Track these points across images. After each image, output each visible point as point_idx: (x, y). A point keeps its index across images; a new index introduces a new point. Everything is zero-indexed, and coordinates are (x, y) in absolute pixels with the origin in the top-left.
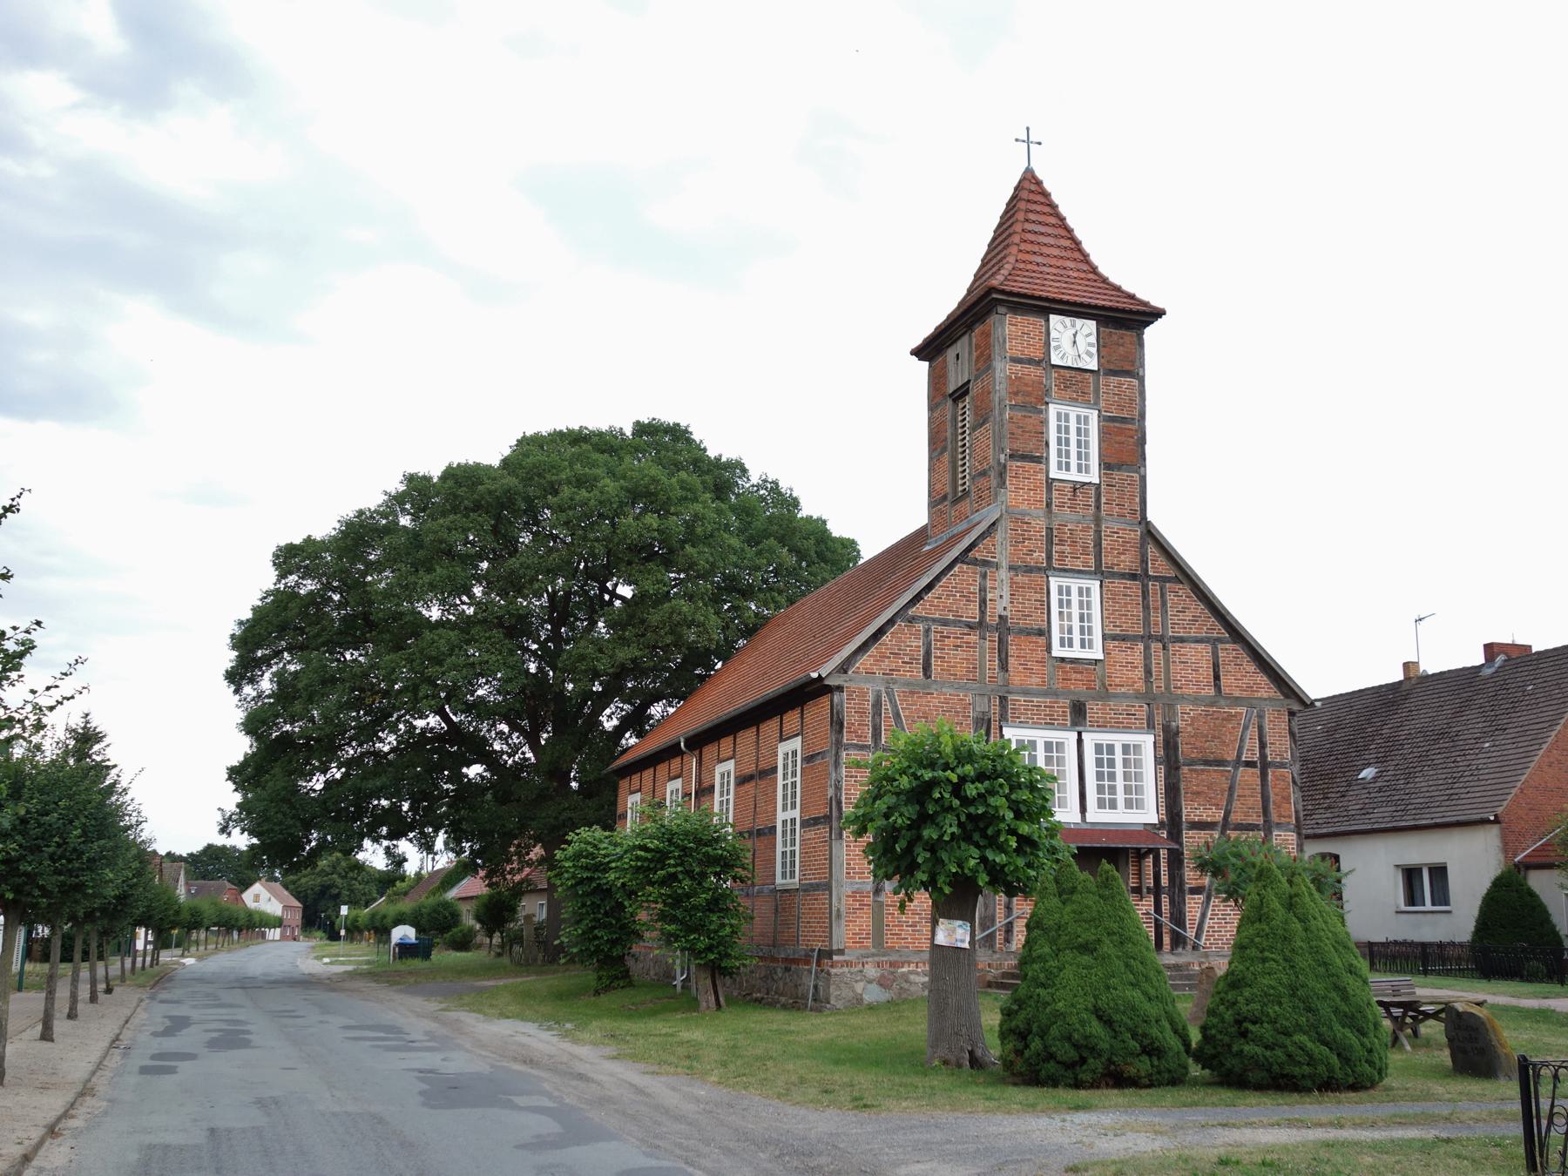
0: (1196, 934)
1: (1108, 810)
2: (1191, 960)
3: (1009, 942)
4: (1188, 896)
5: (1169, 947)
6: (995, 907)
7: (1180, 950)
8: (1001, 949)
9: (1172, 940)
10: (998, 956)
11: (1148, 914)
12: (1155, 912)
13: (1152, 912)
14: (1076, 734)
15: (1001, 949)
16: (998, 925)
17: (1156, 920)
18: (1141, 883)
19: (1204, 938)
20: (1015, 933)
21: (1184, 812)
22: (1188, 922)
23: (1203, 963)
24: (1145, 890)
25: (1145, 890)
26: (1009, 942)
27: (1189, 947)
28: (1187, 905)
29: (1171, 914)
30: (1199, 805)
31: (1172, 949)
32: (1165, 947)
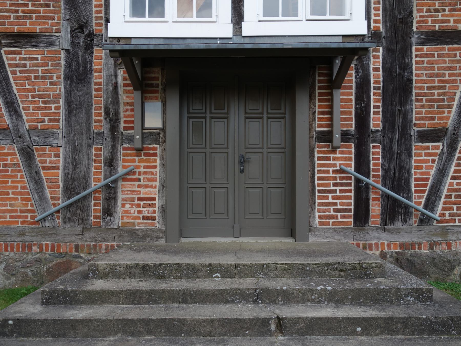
0: (428, 200)
1: (147, 18)
2: (417, 240)
3: (111, 215)
4: (415, 146)
5: (379, 220)
6: (89, 165)
7: (398, 224)
8: (97, 224)
9: (383, 210)
10: (92, 234)
11: (342, 171)
12: (358, 169)
13: (352, 169)
14: (245, 33)
15: (97, 224)
16: (93, 186)
17: (358, 181)
18: (331, 126)
19: (441, 206)
20: (120, 202)
21: (416, 15)
22: (413, 183)
23: (437, 243)
24: (337, 136)
25: (337, 136)
26: (111, 215)
27: (414, 220)
28: (414, 158)
29: (386, 172)
30: (443, 4)
31: (384, 223)
32: (371, 220)
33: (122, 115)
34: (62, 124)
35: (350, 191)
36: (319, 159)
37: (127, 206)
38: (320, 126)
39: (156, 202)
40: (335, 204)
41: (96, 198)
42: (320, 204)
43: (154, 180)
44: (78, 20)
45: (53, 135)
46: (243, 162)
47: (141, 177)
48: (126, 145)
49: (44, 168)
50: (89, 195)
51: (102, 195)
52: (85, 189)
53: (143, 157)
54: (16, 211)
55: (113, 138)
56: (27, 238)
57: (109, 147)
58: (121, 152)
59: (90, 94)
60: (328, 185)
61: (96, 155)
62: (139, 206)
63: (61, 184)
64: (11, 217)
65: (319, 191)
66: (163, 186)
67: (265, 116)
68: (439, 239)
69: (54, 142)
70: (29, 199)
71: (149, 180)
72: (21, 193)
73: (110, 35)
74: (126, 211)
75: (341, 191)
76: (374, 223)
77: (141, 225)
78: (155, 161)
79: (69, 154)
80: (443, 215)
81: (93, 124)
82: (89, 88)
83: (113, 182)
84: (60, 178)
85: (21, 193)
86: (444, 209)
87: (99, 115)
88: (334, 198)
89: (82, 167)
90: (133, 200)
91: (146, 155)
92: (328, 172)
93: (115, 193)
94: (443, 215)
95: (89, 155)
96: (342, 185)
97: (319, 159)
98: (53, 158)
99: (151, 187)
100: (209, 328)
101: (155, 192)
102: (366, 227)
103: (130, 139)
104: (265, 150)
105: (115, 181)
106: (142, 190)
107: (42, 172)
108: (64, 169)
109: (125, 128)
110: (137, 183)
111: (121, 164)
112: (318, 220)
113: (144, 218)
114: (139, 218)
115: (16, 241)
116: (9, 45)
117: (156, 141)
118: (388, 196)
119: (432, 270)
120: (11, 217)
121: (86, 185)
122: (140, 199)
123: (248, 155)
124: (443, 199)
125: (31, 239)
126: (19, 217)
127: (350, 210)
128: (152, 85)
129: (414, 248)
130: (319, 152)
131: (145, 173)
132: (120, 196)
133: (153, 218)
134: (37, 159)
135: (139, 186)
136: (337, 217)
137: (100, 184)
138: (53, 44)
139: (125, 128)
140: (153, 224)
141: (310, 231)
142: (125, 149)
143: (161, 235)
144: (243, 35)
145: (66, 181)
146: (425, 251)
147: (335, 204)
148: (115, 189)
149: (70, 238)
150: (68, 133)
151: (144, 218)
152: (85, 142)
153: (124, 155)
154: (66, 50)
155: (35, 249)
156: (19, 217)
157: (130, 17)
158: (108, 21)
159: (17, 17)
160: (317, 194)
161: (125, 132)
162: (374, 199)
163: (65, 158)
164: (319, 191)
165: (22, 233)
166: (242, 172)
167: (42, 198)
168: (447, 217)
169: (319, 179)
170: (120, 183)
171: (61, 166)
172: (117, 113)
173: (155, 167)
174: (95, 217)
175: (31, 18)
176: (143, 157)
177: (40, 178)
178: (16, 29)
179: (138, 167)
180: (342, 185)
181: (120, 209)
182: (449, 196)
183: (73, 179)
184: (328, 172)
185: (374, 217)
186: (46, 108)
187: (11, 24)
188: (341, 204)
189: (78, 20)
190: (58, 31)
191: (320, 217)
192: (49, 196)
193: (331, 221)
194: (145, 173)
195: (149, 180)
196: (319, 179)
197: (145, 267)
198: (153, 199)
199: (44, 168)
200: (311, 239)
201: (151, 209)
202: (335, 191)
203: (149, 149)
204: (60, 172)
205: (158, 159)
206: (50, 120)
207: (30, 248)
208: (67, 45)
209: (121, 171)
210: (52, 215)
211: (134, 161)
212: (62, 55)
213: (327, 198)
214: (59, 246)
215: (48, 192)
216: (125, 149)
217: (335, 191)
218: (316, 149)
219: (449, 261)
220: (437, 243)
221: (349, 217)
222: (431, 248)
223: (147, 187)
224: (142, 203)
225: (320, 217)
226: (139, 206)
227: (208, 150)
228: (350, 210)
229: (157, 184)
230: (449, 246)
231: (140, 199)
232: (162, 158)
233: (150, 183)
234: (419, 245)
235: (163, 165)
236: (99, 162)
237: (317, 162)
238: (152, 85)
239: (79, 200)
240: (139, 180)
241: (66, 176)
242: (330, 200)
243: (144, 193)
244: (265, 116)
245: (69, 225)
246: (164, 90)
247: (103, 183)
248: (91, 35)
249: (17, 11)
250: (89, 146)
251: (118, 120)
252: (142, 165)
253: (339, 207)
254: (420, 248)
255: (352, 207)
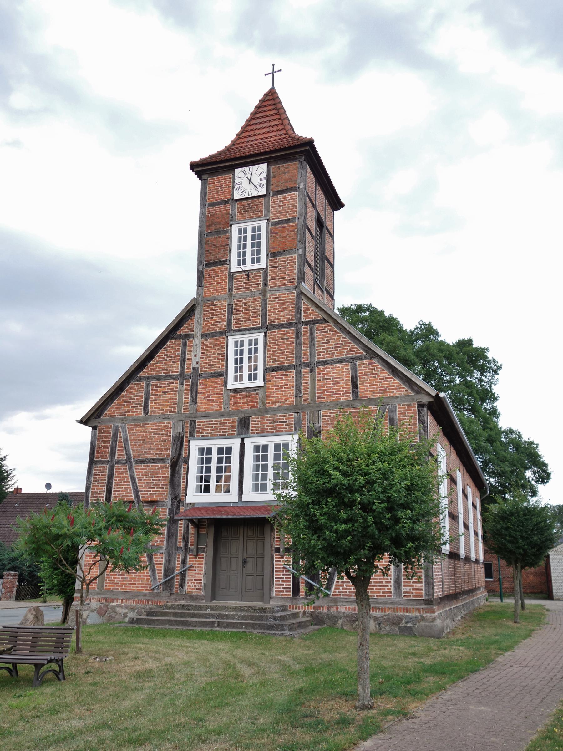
5: (304, 594)
6: (175, 562)
10: (174, 597)
16: (176, 572)
19: (334, 587)
20: (187, 581)
33: (190, 539)
34: (165, 543)
35: (290, 578)
36: (276, 561)
37: (190, 583)
38: (277, 544)
39: (202, 582)
40: (283, 585)
41: (177, 579)
42: (276, 585)
43: (201, 570)
44: (175, 494)
45: (161, 548)
46: (245, 562)
47: (196, 569)
48: (191, 553)
49: (156, 564)
50: (173, 578)
51: (179, 578)
52: (172, 574)
53: (197, 559)
54: (143, 584)
55: (186, 550)
56: (147, 598)
57: (184, 554)
58: (189, 557)
59: (177, 529)
60: (280, 575)
61: (178, 558)
62: (194, 583)
63: (163, 572)
64: (142, 587)
65: (276, 578)
66: (205, 574)
67: (256, 538)
68: (333, 605)
69: (161, 552)
70: (149, 579)
71: (200, 570)
72: (146, 576)
73: (187, 502)
74: (189, 586)
75: (286, 578)
76: (302, 595)
77: (195, 593)
78: (203, 561)
79: (167, 558)
80: (335, 592)
81: (178, 543)
82: (177, 526)
83: (183, 571)
84: (163, 569)
85: (146, 576)
86: (335, 589)
87: (180, 539)
88: (282, 581)
89: (172, 563)
90: (192, 580)
91: (199, 558)
92: (280, 568)
93: (185, 577)
94: (335, 592)
95: (175, 558)
96: (286, 575)
97: (276, 561)
98: (160, 559)
99: (200, 574)
100: (195, 624)
101: (201, 576)
102: (298, 597)
103: (192, 551)
104: (256, 556)
105: (185, 571)
106: (197, 575)
107: (155, 566)
108: (165, 564)
109: (191, 545)
110: (194, 572)
111: (188, 562)
112: (275, 593)
113: (197, 589)
114: (194, 589)
115: (143, 599)
116: (146, 506)
117: (203, 552)
118: (308, 582)
119: (328, 621)
120: (142, 587)
121: (173, 572)
122: (195, 580)
123: (248, 559)
124: (335, 584)
125: (149, 598)
126: (145, 587)
127: (290, 588)
128: (203, 525)
129: (320, 609)
130: (276, 558)
131: (198, 567)
132: (187, 578)
133: (200, 590)
134: (154, 559)
135: (195, 573)
136: (283, 591)
137: (178, 572)
138: (164, 506)
139: (191, 545)
140: (200, 592)
141: (271, 598)
142: (190, 555)
143: (203, 598)
144: (243, 500)
145: (165, 570)
146: (325, 611)
147: (283, 585)
148: (185, 574)
149: (165, 598)
150: (167, 548)
151: (197, 589)
152: (174, 551)
153: (190, 558)
154: (169, 509)
155: (150, 603)
156: (145, 587)
157: (196, 492)
158: (186, 495)
159: (150, 494)
160: (275, 579)
161: (191, 547)
162: (302, 583)
163: (165, 559)
164: (276, 578)
165: (145, 595)
166: (244, 567)
167: (155, 578)
168: (337, 593)
169: (276, 571)
170: (187, 572)
171: (163, 563)
172: (188, 538)
173: (202, 564)
174: (176, 588)
175: (156, 494)
176: (197, 559)
177: (154, 569)
178: (149, 499)
179: (195, 564)
180: (286, 575)
181: (186, 584)
182: (338, 582)
183: (168, 569)
184: (280, 568)
185: (302, 592)
186: (373, 366)
187: (148, 497)
188: (286, 585)
189: (175, 494)
190: (166, 499)
191: (276, 591)
192: (157, 577)
193: (281, 593)
194: (198, 567)
195: (200, 570)
196: (276, 571)
197: (183, 605)
198: (201, 580)
199: (156, 564)
200: (271, 603)
201: (200, 585)
202: (283, 578)
203: (200, 555)
204: (163, 566)
205: (204, 560)
206: (160, 541)
207: (148, 602)
208: (169, 506)
209: (188, 566)
210: (158, 586)
211: (193, 561)
212: (167, 511)
213: (279, 581)
214: (160, 602)
215: (157, 575)
216: (190, 555)
217: (283, 578)
218: (275, 556)
219: (335, 616)
220: (332, 607)
221: (290, 591)
222: (328, 609)
223: (198, 574)
224: (196, 582)
225: (276, 591)
226: (194, 583)
227: (229, 556)
228: (290, 588)
229: (203, 572)
230: (337, 608)
231: (195, 580)
232: (206, 560)
233: (200, 572)
234: (323, 607)
235: (206, 563)
236: (179, 561)
237: (275, 563)
238: (203, 525)
239: (169, 579)
240: (195, 570)
241: (165, 568)
242: (281, 583)
243: (197, 576)
244: (256, 538)
245: (165, 592)
246: (208, 527)
247: (180, 571)
248: (179, 501)
249: (150, 491)
250: (176, 554)
251: (188, 541)
252: (197, 563)
253: (285, 586)
254: (323, 609)
255: (291, 587)
